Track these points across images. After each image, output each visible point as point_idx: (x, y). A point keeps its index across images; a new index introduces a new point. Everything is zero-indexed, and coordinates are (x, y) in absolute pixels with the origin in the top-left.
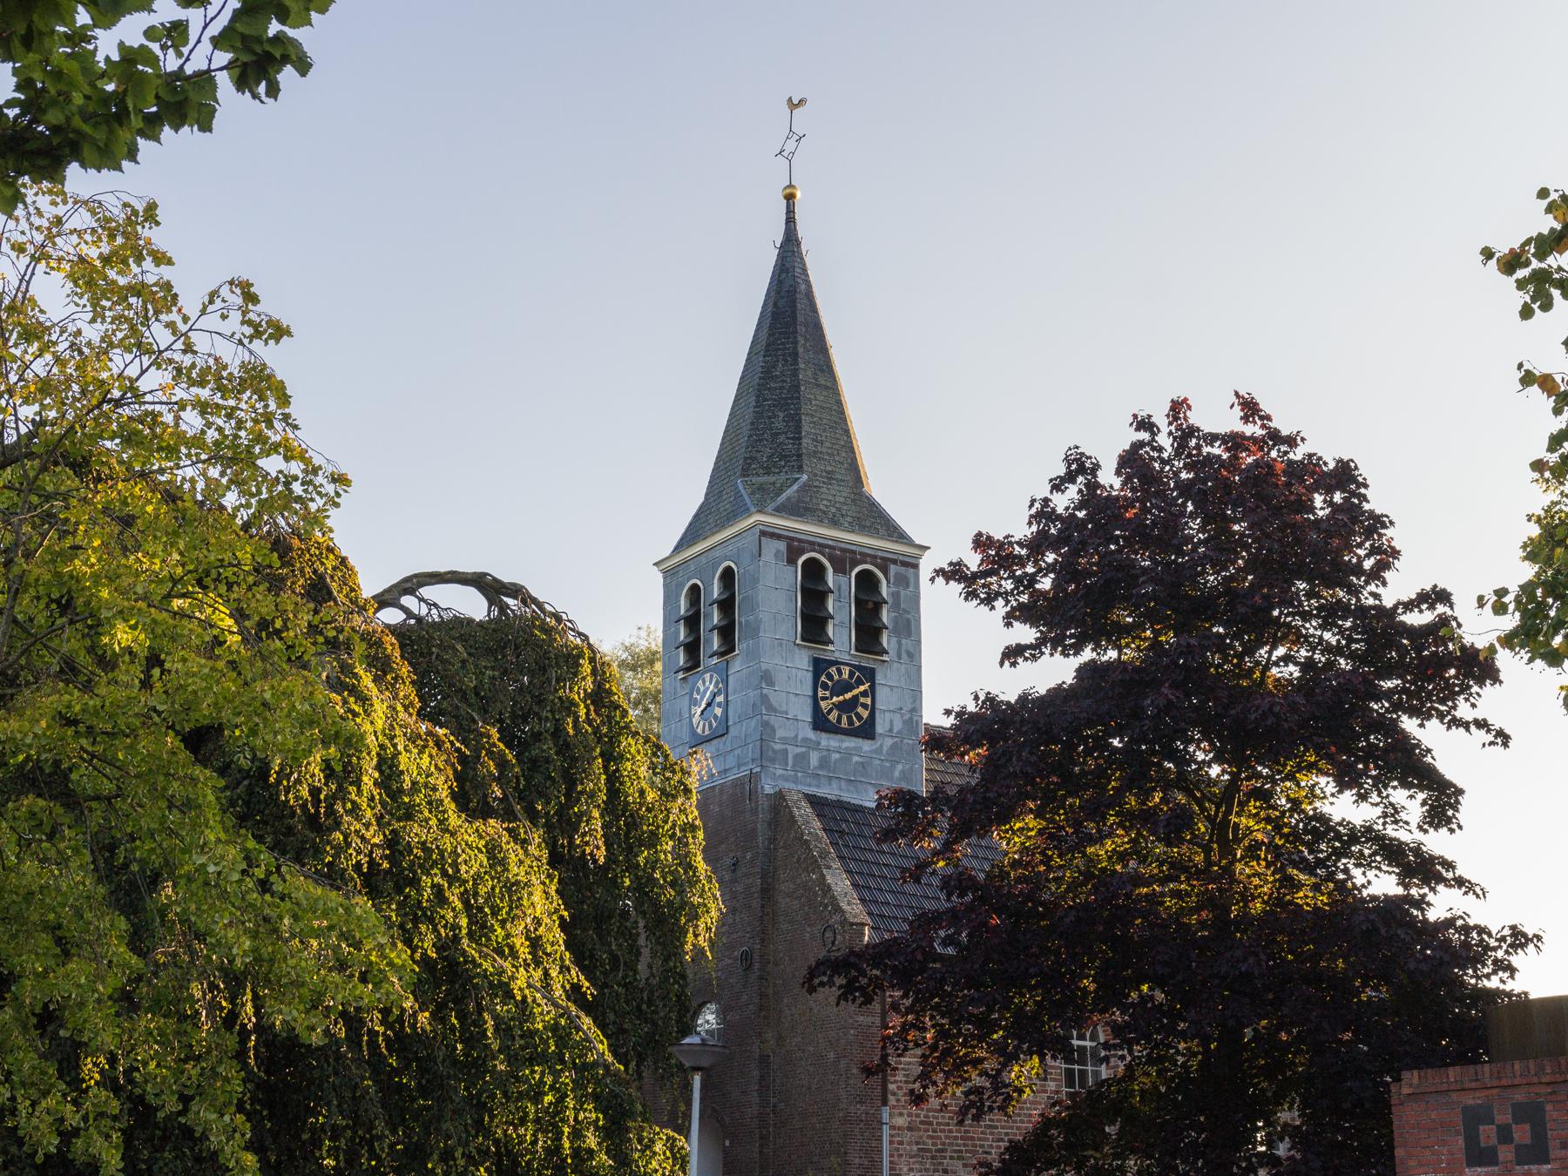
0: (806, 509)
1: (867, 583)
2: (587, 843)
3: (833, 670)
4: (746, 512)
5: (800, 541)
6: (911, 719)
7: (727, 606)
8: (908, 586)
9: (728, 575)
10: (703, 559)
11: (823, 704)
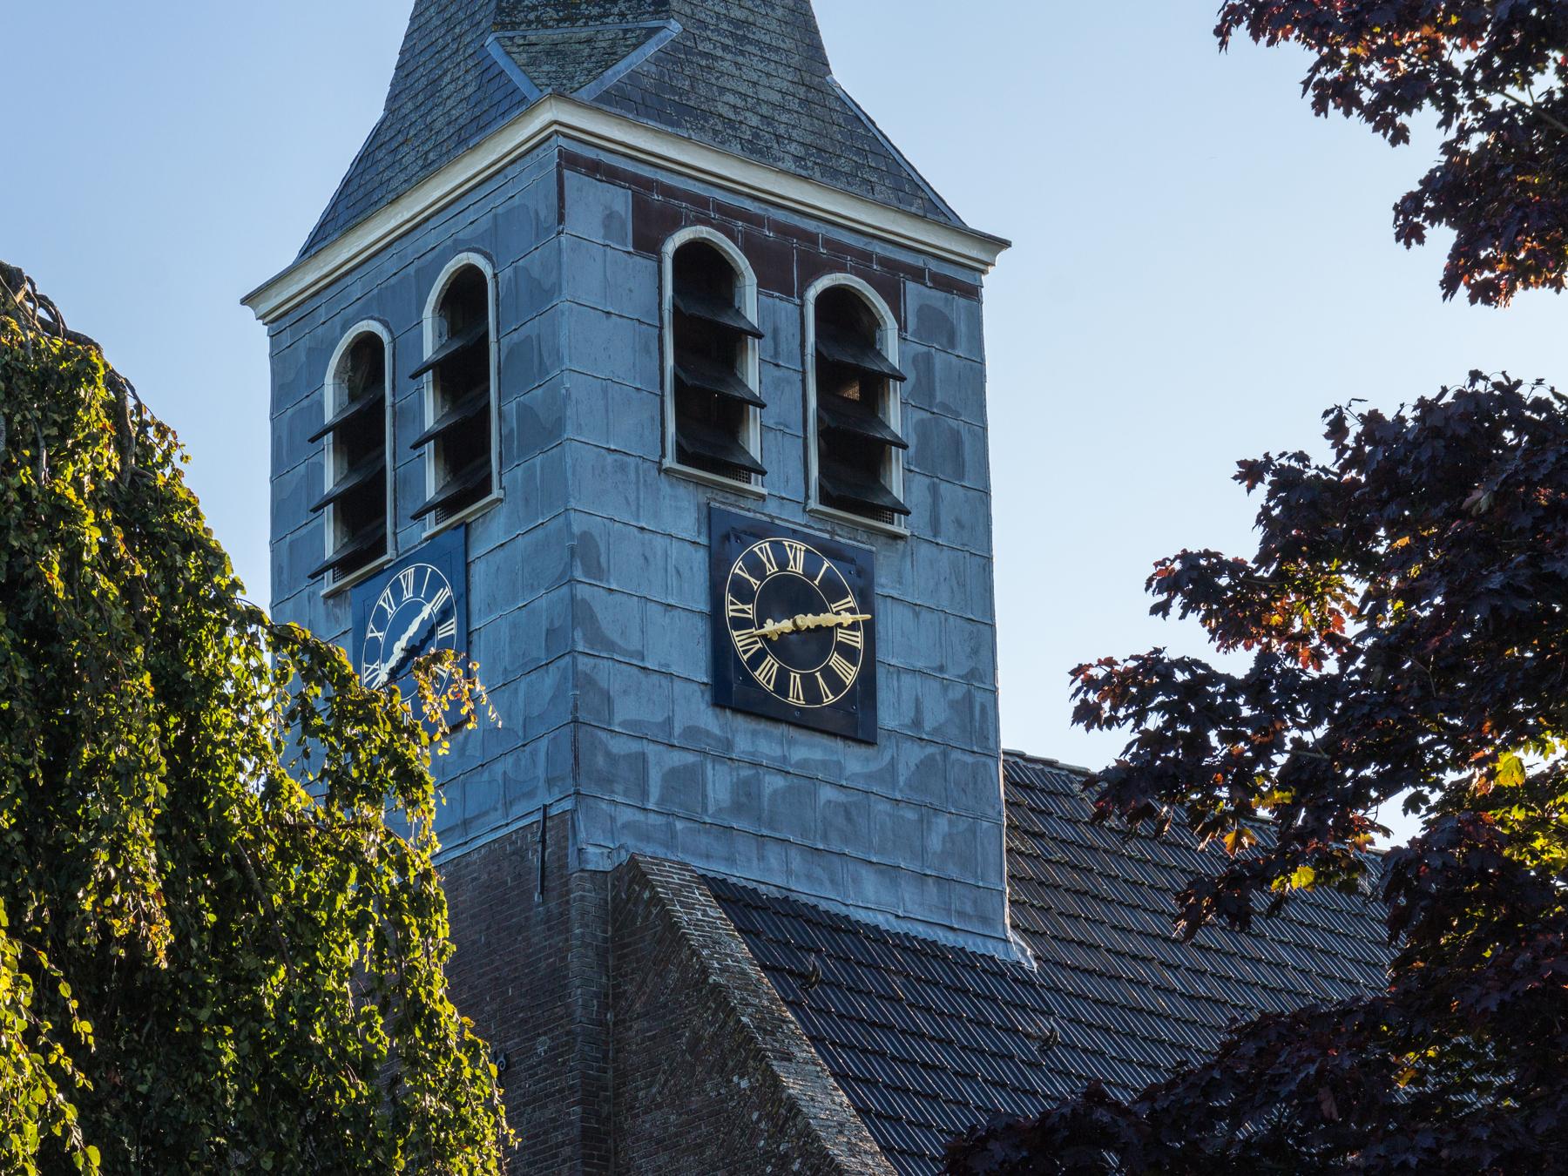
0: (685, 109)
1: (844, 319)
2: (117, 911)
3: (762, 549)
4: (519, 105)
5: (668, 191)
6: (969, 699)
7: (462, 374)
8: (952, 341)
9: (465, 297)
10: (389, 264)
11: (739, 638)
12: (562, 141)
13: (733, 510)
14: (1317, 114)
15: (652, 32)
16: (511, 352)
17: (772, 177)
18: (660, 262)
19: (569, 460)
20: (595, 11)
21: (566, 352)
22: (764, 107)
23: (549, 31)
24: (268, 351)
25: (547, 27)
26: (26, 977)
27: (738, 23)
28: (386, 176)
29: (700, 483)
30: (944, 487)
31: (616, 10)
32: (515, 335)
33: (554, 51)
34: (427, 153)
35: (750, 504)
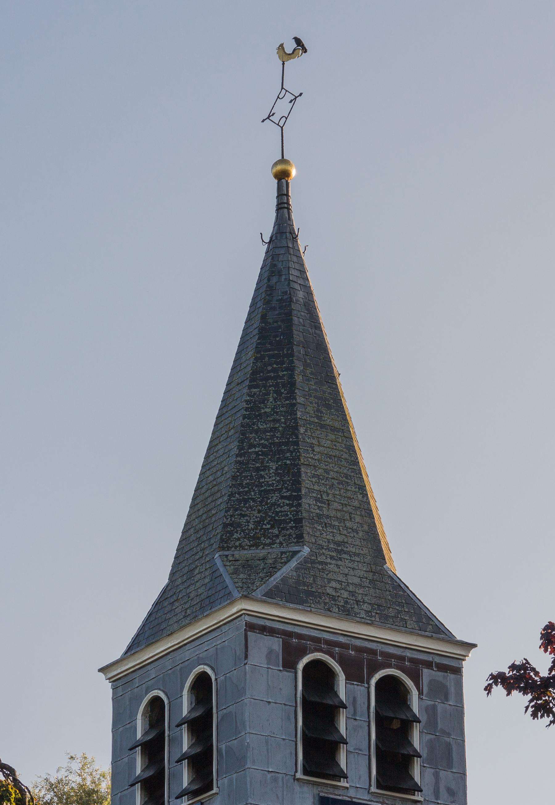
0: (310, 594)
1: (391, 693)
4: (228, 598)
5: (300, 636)
7: (200, 726)
8: (447, 698)
9: (202, 685)
10: (168, 663)
12: (247, 618)
13: (332, 796)
14: (534, 719)
15: (295, 553)
16: (223, 717)
17: (353, 625)
18: (296, 673)
19: (248, 779)
20: (268, 541)
21: (247, 724)
22: (351, 586)
23: (246, 552)
24: (111, 696)
25: (245, 549)
27: (338, 544)
28: (168, 616)
29: (314, 784)
30: (442, 774)
31: (278, 541)
32: (225, 711)
33: (247, 565)
34: (186, 609)
35: (340, 792)
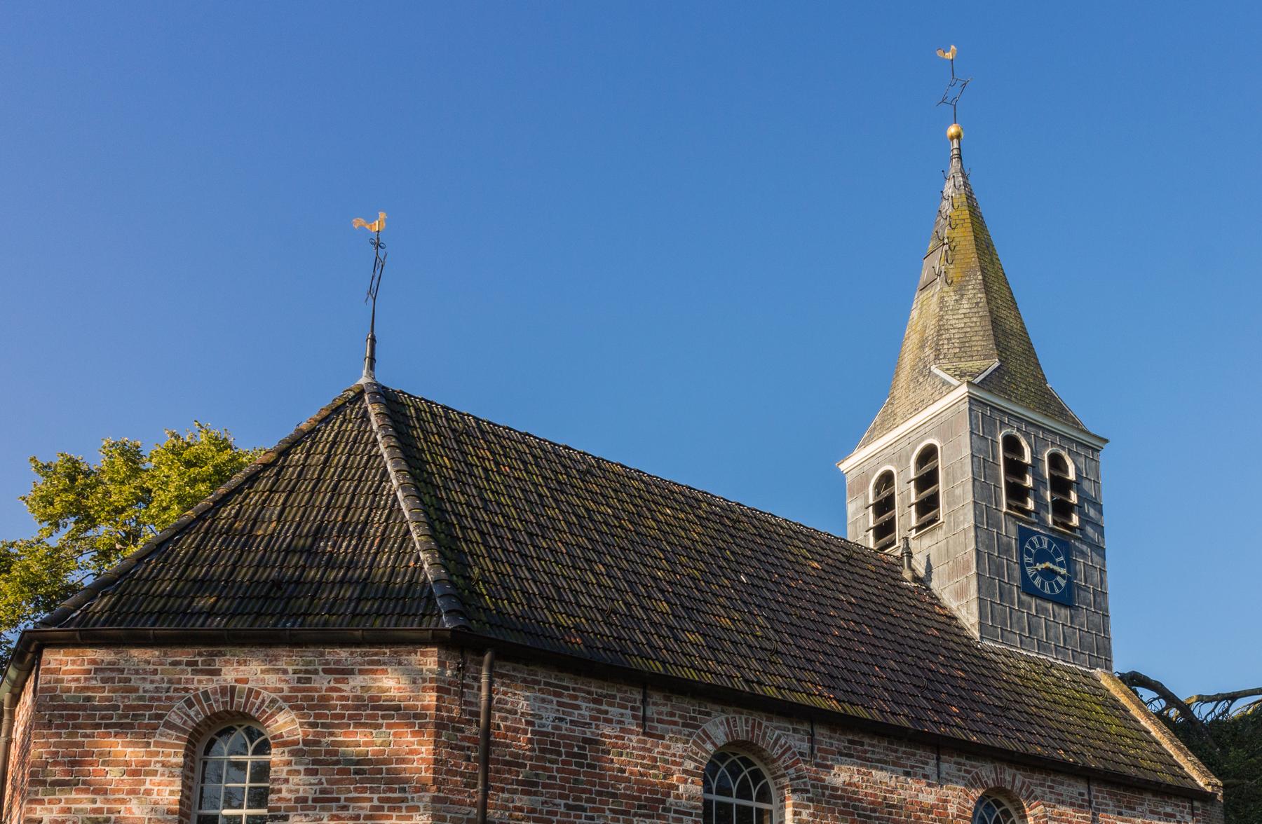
3: (1034, 539)
26: (1196, 804)
